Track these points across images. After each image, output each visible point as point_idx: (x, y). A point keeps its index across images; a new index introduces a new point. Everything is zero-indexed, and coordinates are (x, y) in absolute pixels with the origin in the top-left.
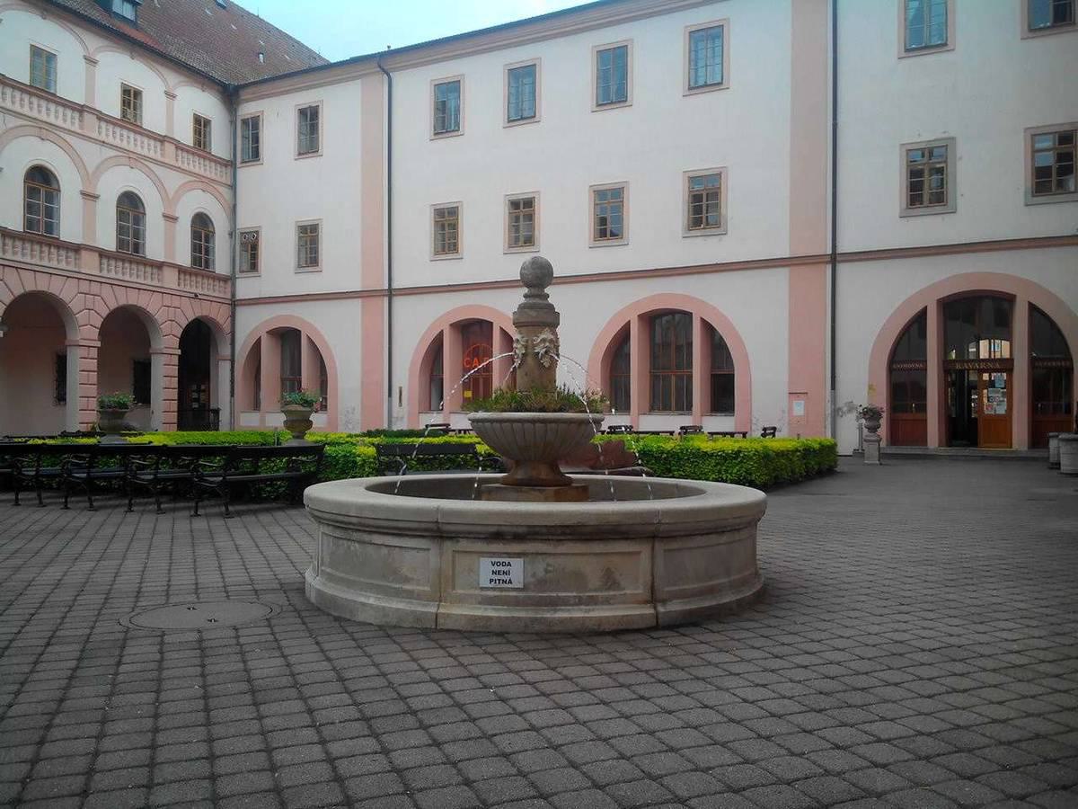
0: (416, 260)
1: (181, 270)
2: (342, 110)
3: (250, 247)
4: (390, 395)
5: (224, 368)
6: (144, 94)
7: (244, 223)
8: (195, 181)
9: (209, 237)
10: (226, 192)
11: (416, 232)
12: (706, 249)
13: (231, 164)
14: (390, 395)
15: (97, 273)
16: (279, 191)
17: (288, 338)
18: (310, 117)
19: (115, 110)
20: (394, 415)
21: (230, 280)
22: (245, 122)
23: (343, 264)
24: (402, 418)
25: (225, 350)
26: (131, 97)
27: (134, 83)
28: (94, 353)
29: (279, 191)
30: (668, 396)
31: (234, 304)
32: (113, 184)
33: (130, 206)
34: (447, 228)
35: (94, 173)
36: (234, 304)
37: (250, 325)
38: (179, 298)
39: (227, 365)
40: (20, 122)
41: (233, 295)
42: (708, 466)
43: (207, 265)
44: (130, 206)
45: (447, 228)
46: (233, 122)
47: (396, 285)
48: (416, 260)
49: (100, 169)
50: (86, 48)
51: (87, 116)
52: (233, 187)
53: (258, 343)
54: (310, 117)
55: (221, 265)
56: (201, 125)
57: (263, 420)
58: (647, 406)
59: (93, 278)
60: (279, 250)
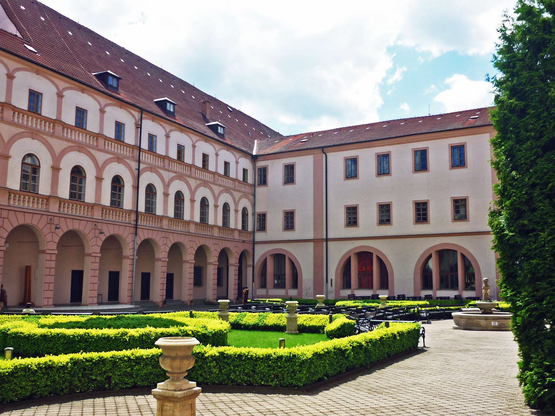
0: (337, 226)
1: (219, 228)
2: (304, 165)
3: (262, 219)
4: (327, 282)
5: (250, 270)
6: (230, 164)
7: (259, 209)
8: (25, 132)
9: (36, 169)
10: (251, 197)
11: (337, 217)
12: (461, 227)
13: (254, 186)
14: (327, 282)
15: (101, 218)
16: (275, 198)
17: (279, 258)
18: (290, 171)
19: (24, 106)
20: (329, 290)
21: (253, 233)
22: (260, 169)
23: (304, 228)
24: (332, 292)
25: (250, 262)
26: (35, 97)
27: (121, 120)
28: (98, 260)
29: (275, 198)
30: (365, 283)
31: (254, 243)
32: (70, 160)
33: (78, 173)
34: (352, 216)
35: (102, 167)
36: (254, 243)
37: (260, 252)
38: (71, 220)
39: (251, 269)
40: (70, 144)
41: (254, 240)
42: (303, 376)
43: (119, 205)
44: (78, 173)
45: (352, 216)
46: (254, 169)
47: (330, 236)
48: (337, 226)
49: (64, 152)
50: (215, 149)
51: (216, 176)
52: (254, 195)
53: (266, 259)
54: (290, 171)
55: (250, 228)
56: (119, 127)
57: (287, 293)
58: (439, 287)
59: (4, 207)
60: (275, 223)
